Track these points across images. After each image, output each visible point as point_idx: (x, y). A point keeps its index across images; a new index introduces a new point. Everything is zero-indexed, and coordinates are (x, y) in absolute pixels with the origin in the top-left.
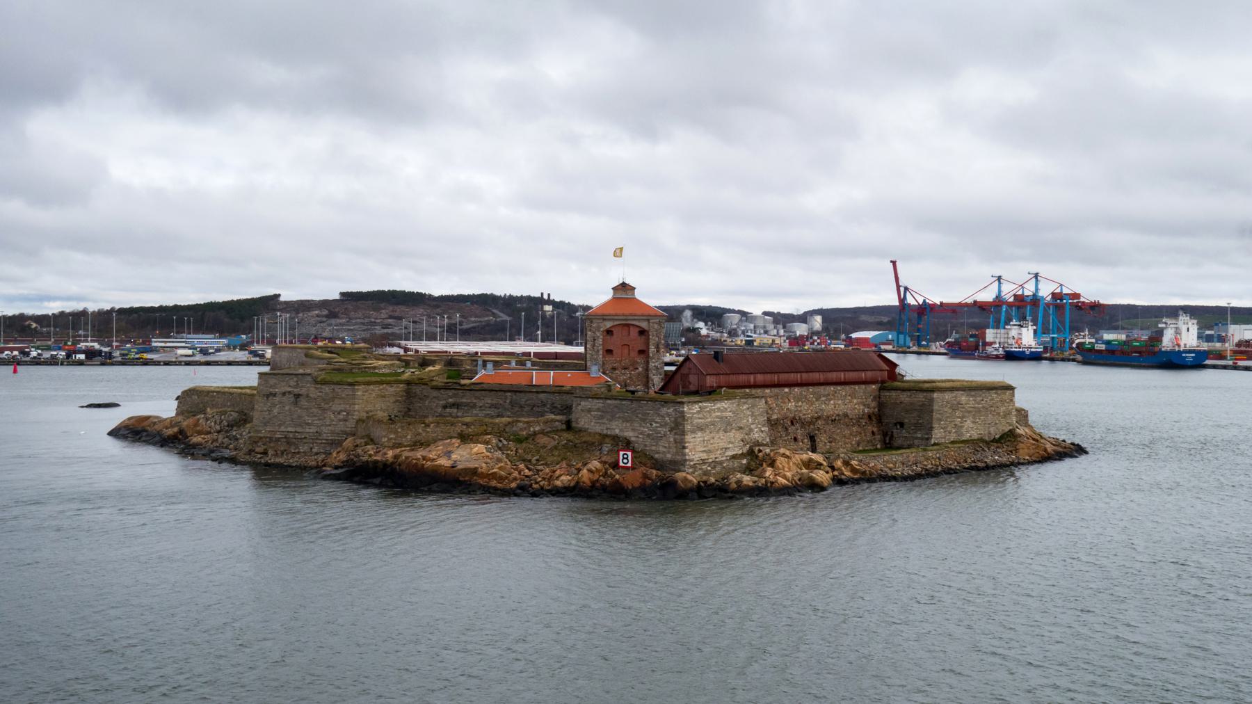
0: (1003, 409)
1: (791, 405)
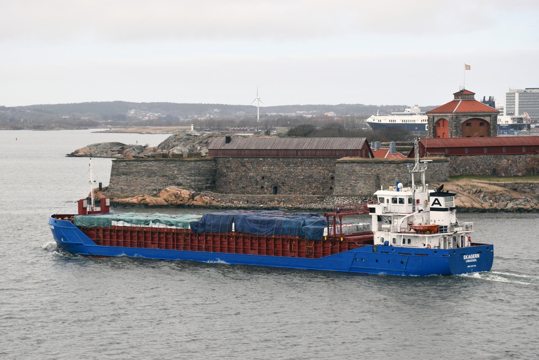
0: (388, 176)
1: (265, 168)
